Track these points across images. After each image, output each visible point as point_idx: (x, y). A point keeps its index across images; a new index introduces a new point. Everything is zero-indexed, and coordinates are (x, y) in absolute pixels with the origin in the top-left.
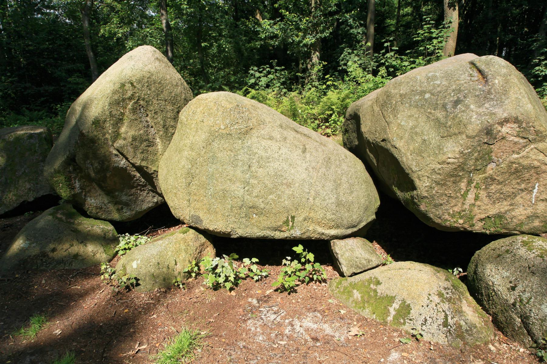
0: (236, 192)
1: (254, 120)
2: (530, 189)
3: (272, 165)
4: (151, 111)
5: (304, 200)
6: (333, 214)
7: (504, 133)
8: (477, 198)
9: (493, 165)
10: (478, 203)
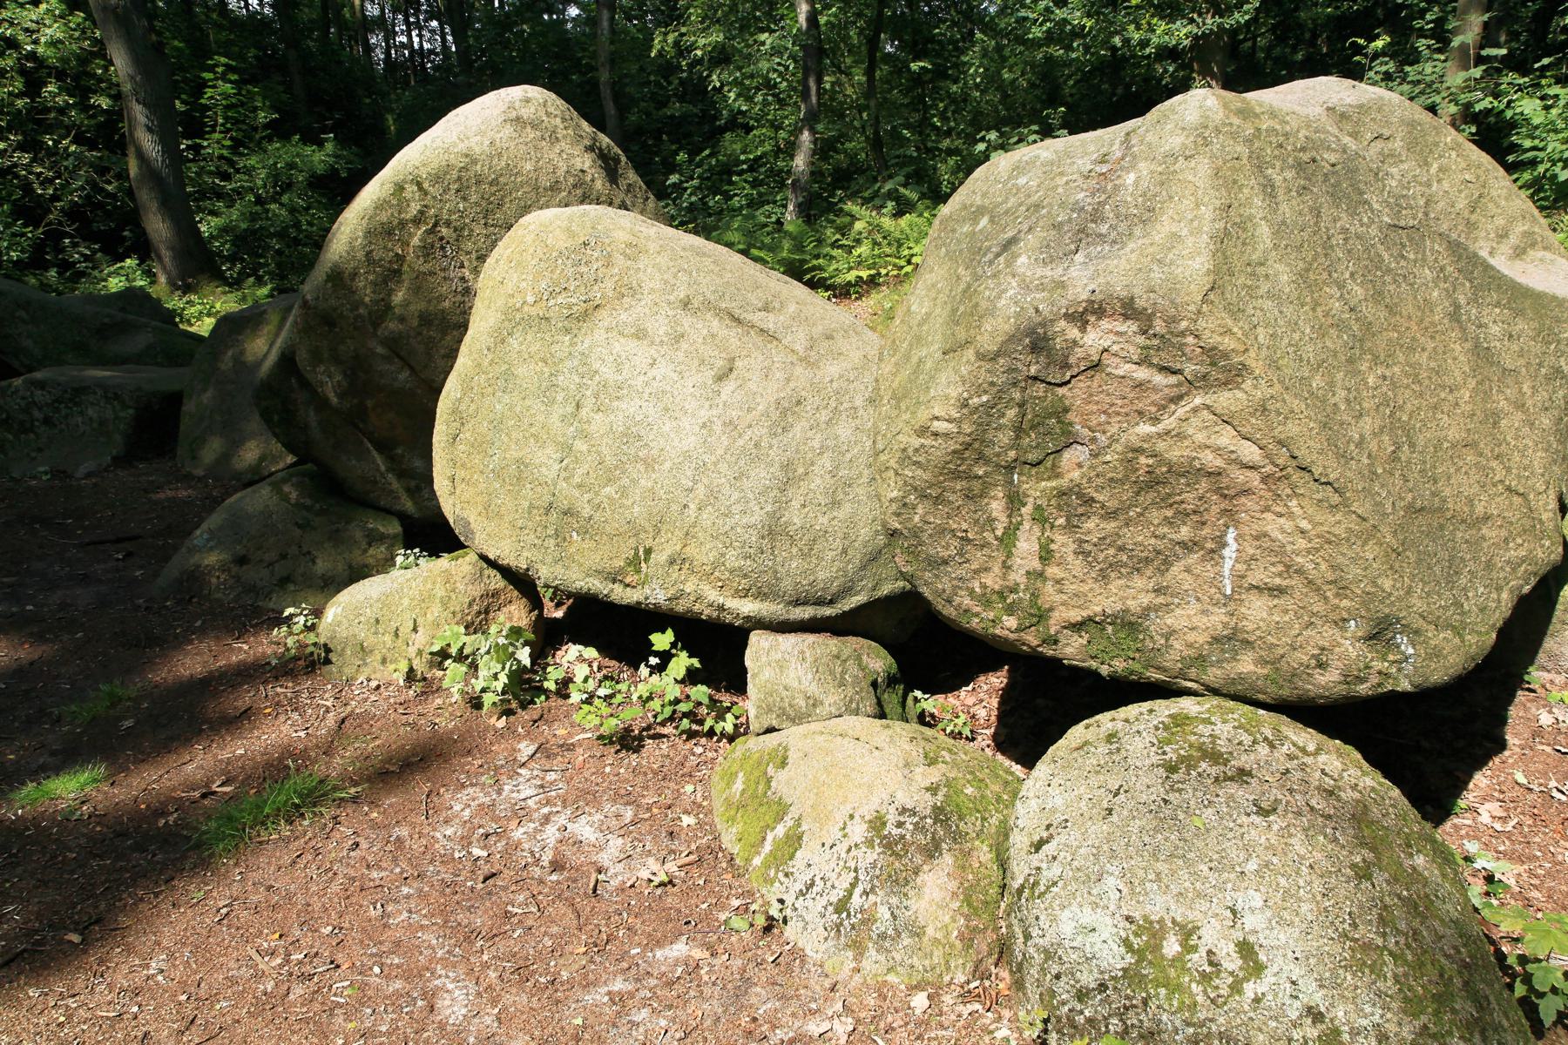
0: (544, 469)
1: (609, 284)
2: (1209, 545)
3: (624, 406)
4: (468, 253)
5: (674, 507)
6: (747, 557)
7: (1092, 351)
8: (1046, 555)
9: (1071, 456)
10: (1053, 571)
